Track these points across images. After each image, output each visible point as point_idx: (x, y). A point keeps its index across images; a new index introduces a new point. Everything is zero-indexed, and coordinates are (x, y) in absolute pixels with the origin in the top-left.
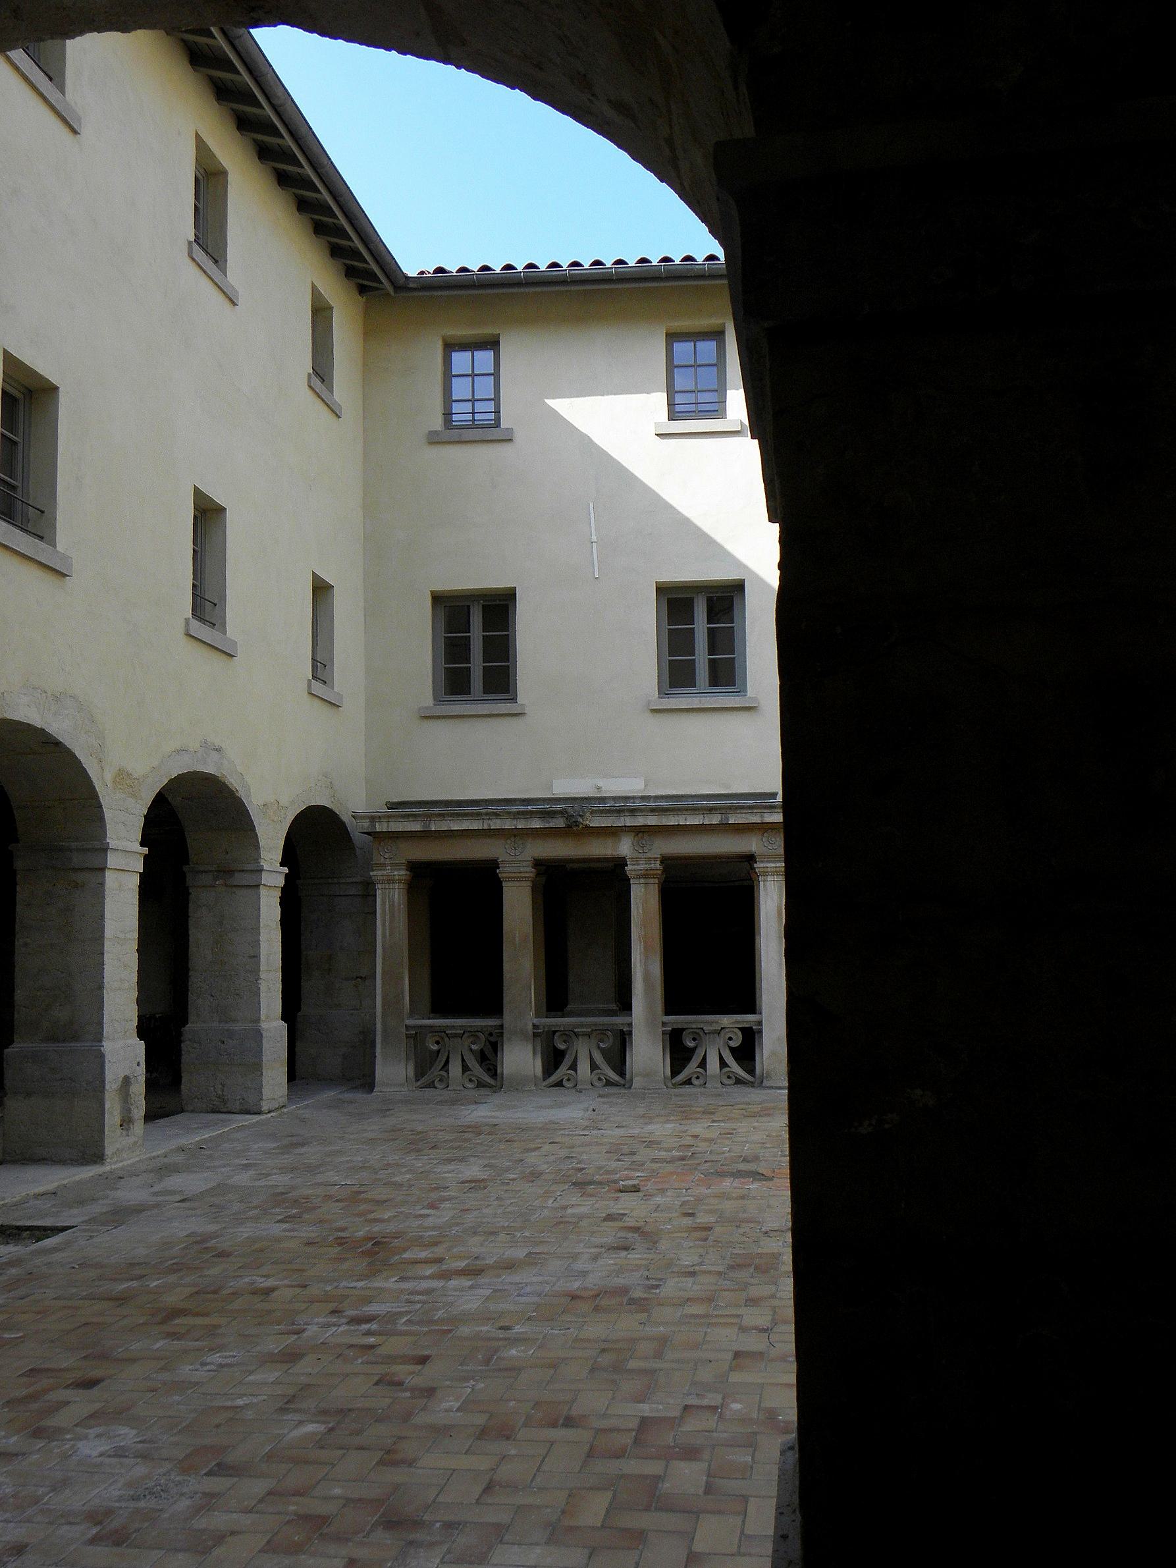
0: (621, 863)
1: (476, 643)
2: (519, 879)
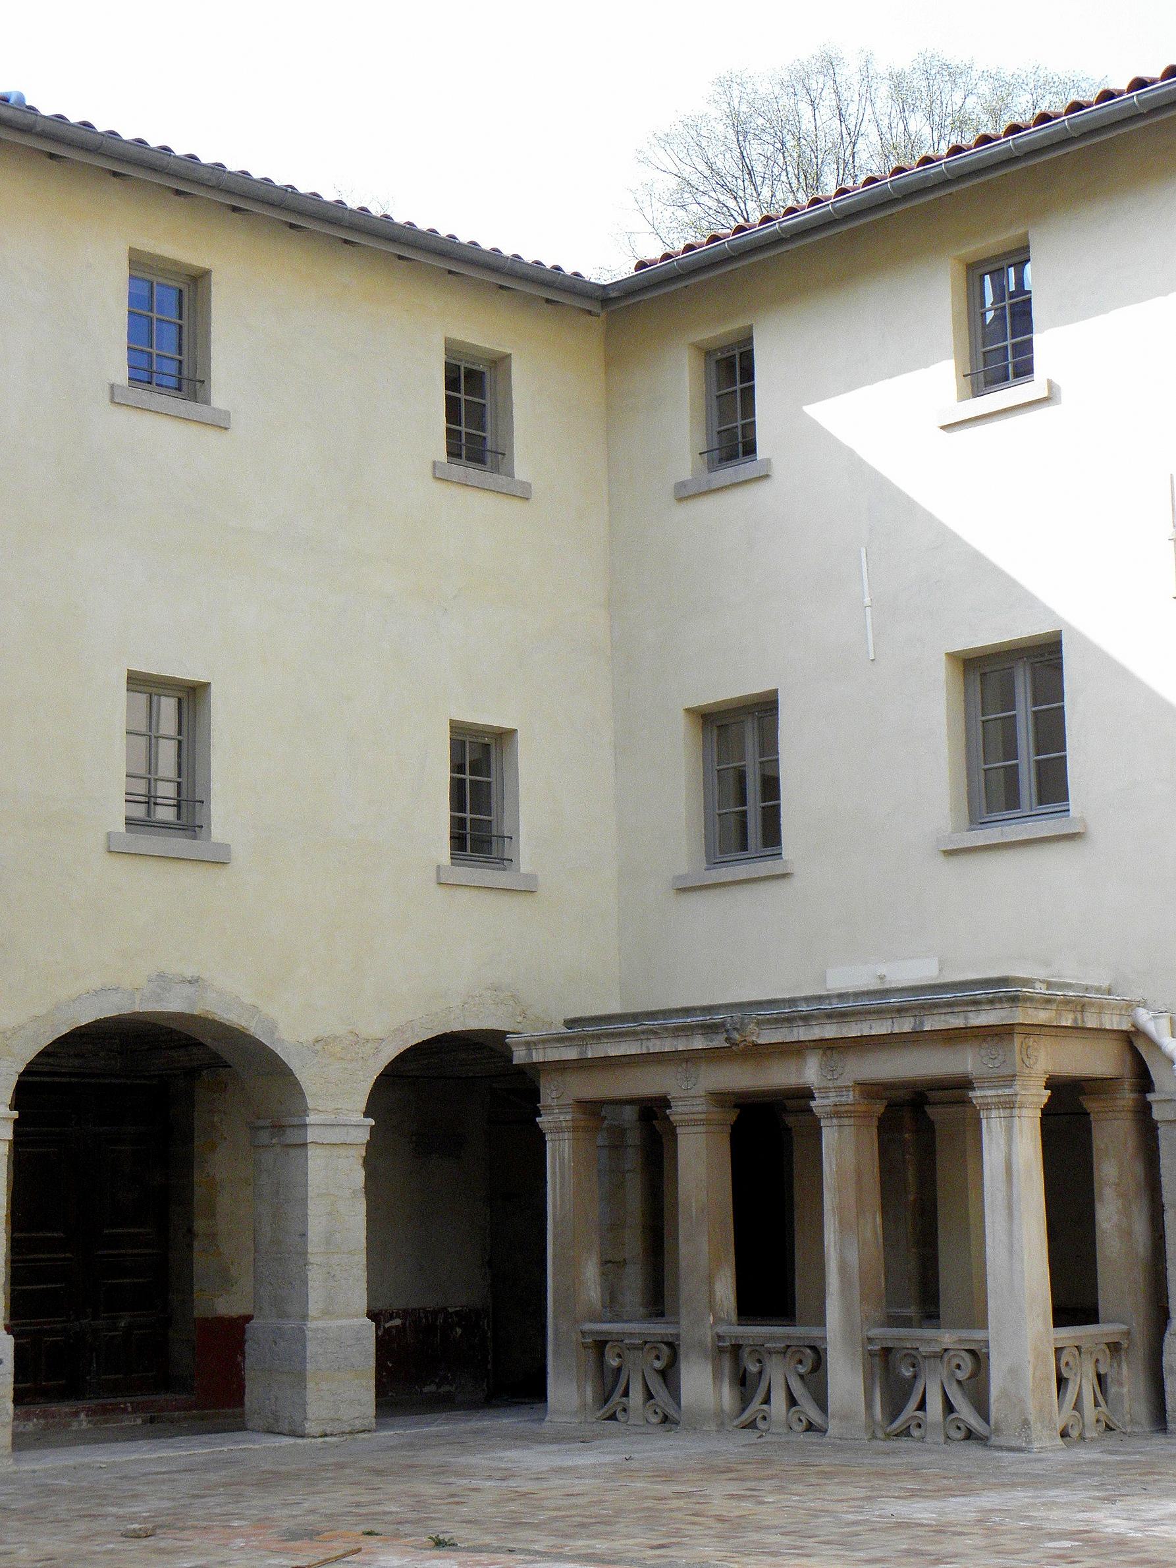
0: (806, 1094)
1: (739, 769)
2: (696, 1123)
